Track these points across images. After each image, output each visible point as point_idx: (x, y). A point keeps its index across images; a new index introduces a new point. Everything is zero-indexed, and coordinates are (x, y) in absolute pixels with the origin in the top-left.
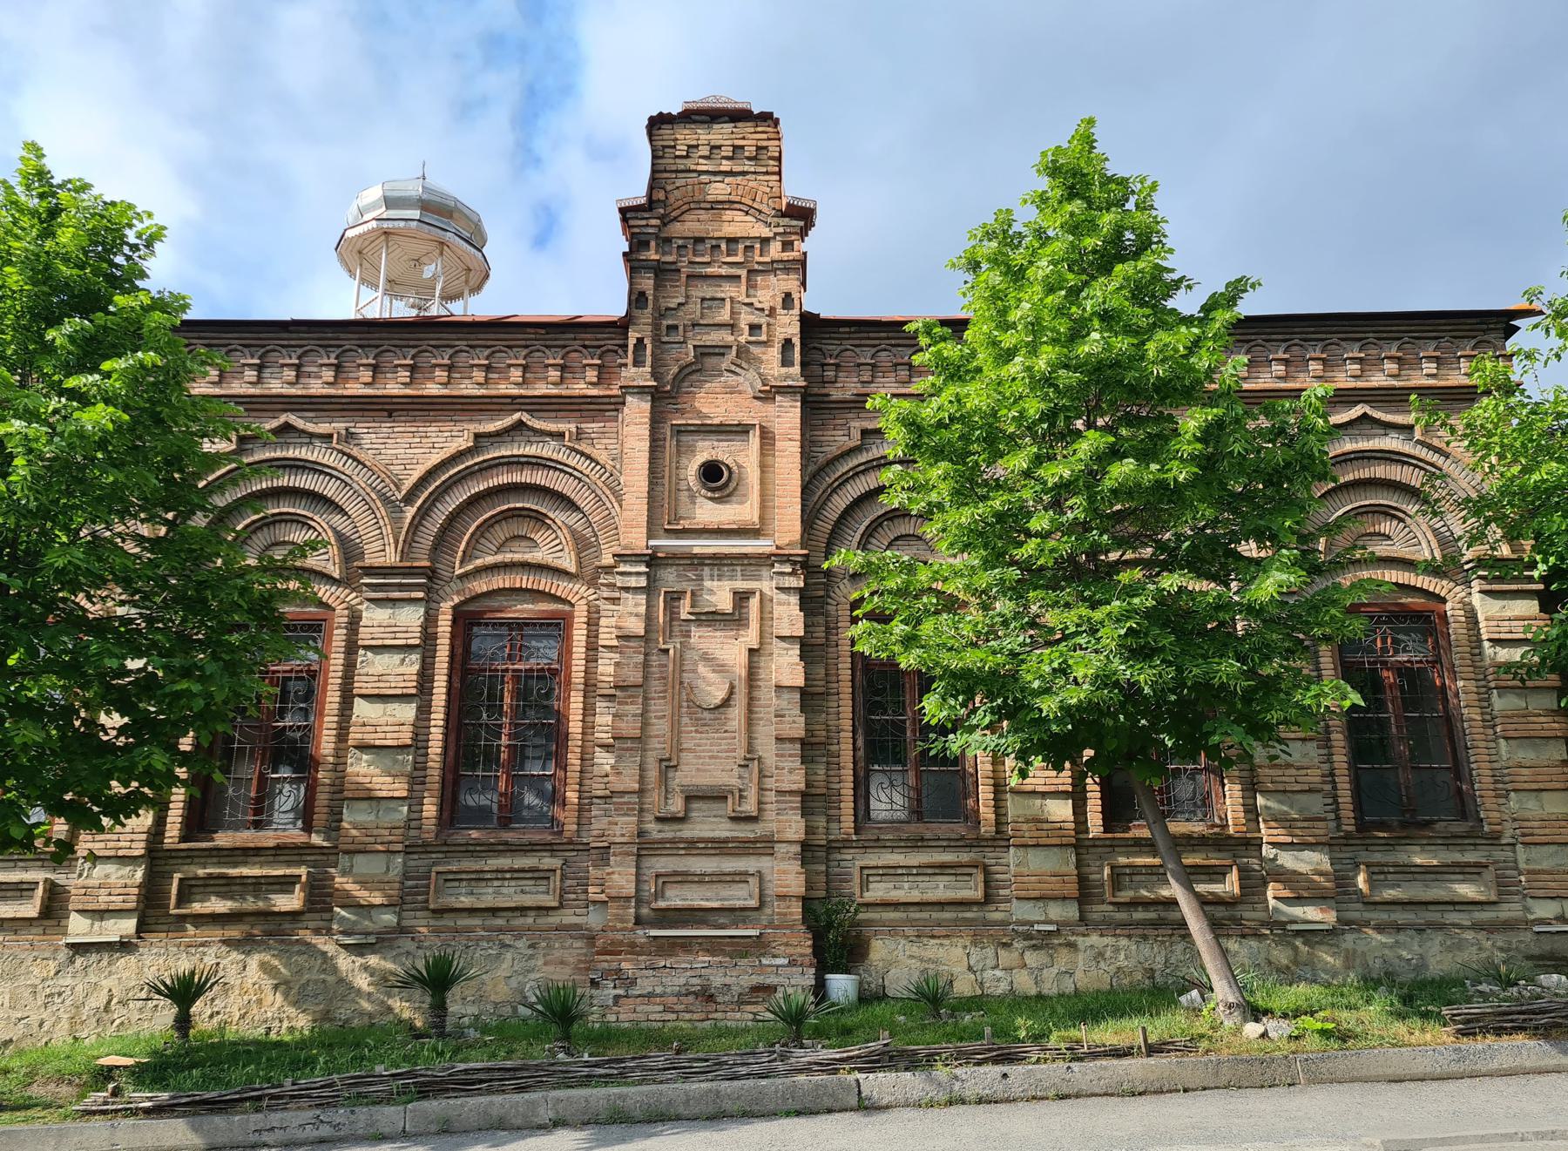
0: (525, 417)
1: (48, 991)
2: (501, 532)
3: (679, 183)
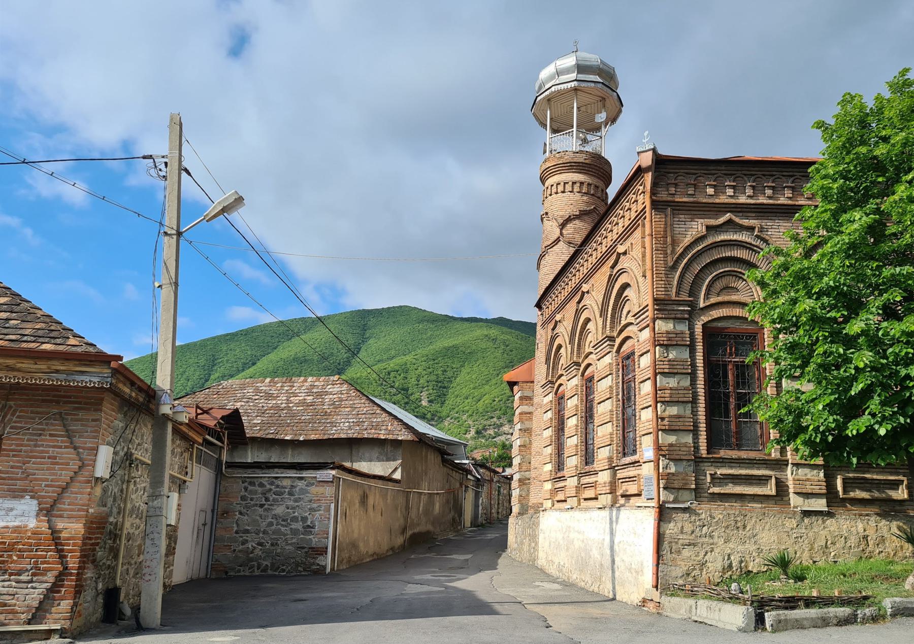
0: (734, 217)
1: (795, 535)
2: (719, 285)
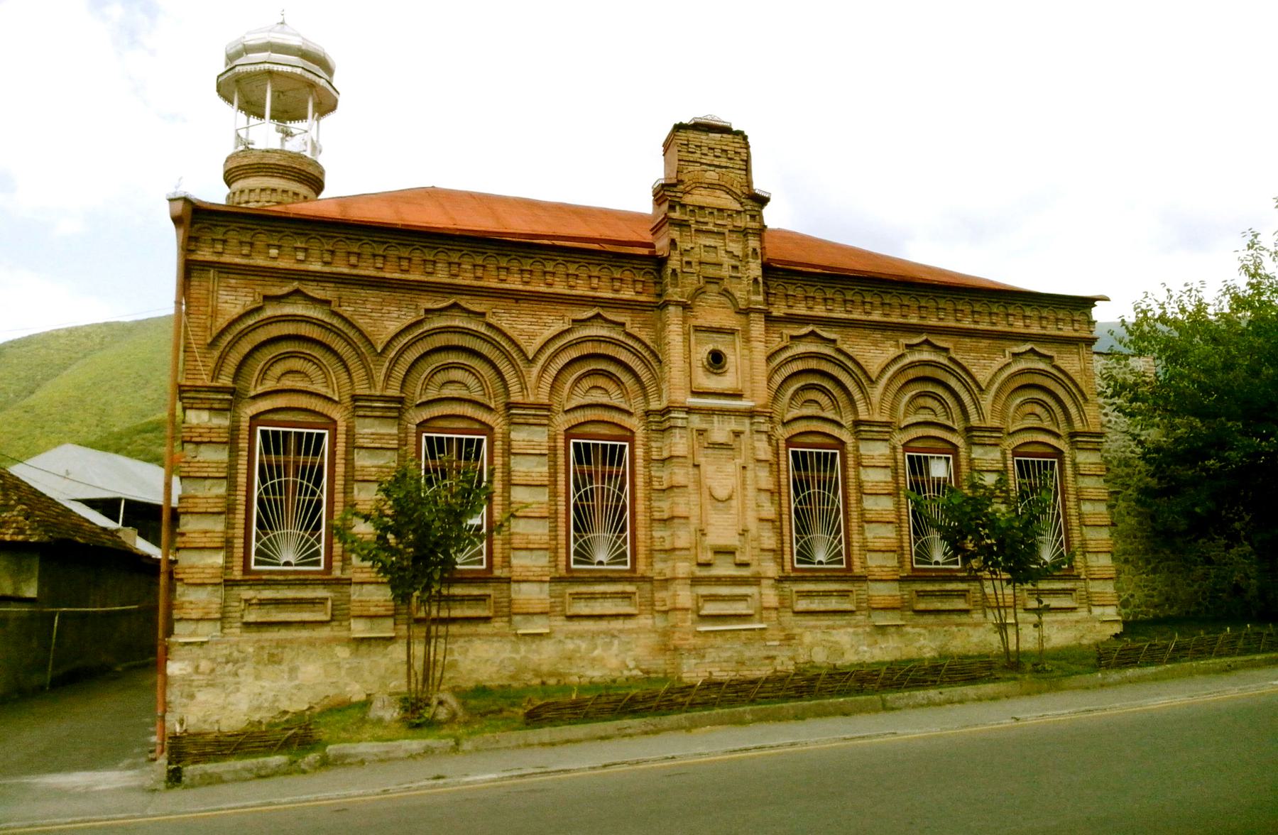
3: (691, 168)
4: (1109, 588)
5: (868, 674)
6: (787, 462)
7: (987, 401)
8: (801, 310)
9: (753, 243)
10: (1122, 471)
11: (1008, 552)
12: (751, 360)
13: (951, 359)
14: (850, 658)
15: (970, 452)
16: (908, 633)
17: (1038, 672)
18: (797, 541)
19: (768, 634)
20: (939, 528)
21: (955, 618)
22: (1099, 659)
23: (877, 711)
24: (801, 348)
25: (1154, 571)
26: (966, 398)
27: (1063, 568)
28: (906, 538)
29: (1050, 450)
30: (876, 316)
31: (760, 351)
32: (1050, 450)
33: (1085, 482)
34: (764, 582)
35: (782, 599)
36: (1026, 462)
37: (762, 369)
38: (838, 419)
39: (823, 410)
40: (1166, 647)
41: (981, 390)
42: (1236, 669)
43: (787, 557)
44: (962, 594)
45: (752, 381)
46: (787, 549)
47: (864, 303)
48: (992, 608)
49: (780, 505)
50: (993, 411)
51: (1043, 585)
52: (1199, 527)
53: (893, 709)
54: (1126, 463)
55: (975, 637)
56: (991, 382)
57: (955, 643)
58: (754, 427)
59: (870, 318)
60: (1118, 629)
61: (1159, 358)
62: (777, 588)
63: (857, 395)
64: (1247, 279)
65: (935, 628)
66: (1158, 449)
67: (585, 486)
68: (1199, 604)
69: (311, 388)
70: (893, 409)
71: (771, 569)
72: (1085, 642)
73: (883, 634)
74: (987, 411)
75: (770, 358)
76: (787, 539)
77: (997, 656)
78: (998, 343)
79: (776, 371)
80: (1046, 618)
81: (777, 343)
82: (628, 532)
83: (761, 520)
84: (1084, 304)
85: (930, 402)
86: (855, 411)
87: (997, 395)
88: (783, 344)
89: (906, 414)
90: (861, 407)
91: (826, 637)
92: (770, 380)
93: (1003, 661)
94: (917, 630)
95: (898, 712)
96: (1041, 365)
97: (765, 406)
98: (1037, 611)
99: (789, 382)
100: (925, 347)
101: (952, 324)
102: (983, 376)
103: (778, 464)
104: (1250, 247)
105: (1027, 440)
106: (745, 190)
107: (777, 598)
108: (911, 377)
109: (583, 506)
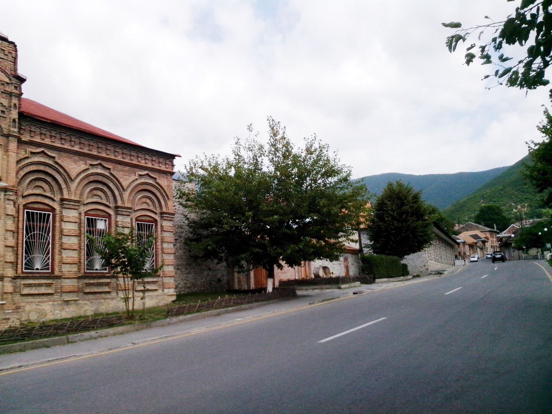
4: (172, 281)
5: (61, 325)
6: (22, 217)
7: (126, 195)
8: (37, 139)
9: (15, 101)
10: (179, 230)
11: (133, 265)
12: (8, 161)
13: (111, 174)
14: (50, 317)
15: (116, 218)
16: (80, 304)
17: (142, 320)
18: (26, 259)
19: (5, 307)
20: (101, 253)
21: (103, 295)
22: (168, 312)
23: (64, 344)
24: (36, 159)
25: (189, 273)
26: (117, 193)
27: (154, 272)
28: (82, 258)
29: (151, 219)
30: (76, 148)
31: (13, 157)
32: (151, 219)
33: (166, 234)
34: (6, 279)
35: (15, 287)
36: (141, 224)
37: (13, 167)
38: (52, 196)
39: (45, 191)
40: (196, 306)
41: (124, 190)
42: (222, 313)
43: (19, 266)
44: (107, 284)
45: (7, 173)
46: (20, 262)
47: (71, 141)
48: (122, 290)
49: (18, 238)
50: (128, 200)
51: (146, 280)
52: (209, 255)
53: (72, 342)
54: (181, 227)
55: (113, 304)
56: (128, 187)
57: (102, 307)
58: (7, 197)
59: (73, 149)
60: (174, 298)
61: (198, 184)
62: (12, 282)
63: (64, 186)
64: (234, 156)
65: (93, 301)
66: (194, 222)
67: (31, 232)
68: (205, 287)
69: (45, 194)
70: (81, 194)
71: (10, 272)
72: (160, 304)
73: (67, 305)
74: (126, 199)
75: (18, 162)
76: (20, 257)
77: (124, 313)
78: (133, 169)
79: (21, 169)
80: (147, 294)
81: (22, 155)
82: (50, 255)
83: (6, 246)
84: (172, 157)
85: (99, 193)
86: (62, 194)
87: (131, 193)
88: (27, 155)
89: (87, 198)
90: (65, 192)
91: (38, 307)
92: (17, 173)
93: (126, 315)
94: (85, 302)
95: (74, 344)
96: (151, 181)
97: (14, 187)
98: (144, 291)
99: (29, 175)
100: (99, 167)
101: (113, 157)
102: (125, 184)
103: (18, 217)
104: (236, 144)
105: (142, 214)
106: (13, 73)
107: (12, 287)
108: (92, 180)
109: (30, 242)
